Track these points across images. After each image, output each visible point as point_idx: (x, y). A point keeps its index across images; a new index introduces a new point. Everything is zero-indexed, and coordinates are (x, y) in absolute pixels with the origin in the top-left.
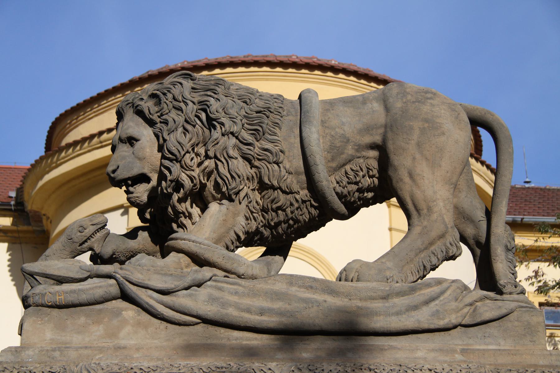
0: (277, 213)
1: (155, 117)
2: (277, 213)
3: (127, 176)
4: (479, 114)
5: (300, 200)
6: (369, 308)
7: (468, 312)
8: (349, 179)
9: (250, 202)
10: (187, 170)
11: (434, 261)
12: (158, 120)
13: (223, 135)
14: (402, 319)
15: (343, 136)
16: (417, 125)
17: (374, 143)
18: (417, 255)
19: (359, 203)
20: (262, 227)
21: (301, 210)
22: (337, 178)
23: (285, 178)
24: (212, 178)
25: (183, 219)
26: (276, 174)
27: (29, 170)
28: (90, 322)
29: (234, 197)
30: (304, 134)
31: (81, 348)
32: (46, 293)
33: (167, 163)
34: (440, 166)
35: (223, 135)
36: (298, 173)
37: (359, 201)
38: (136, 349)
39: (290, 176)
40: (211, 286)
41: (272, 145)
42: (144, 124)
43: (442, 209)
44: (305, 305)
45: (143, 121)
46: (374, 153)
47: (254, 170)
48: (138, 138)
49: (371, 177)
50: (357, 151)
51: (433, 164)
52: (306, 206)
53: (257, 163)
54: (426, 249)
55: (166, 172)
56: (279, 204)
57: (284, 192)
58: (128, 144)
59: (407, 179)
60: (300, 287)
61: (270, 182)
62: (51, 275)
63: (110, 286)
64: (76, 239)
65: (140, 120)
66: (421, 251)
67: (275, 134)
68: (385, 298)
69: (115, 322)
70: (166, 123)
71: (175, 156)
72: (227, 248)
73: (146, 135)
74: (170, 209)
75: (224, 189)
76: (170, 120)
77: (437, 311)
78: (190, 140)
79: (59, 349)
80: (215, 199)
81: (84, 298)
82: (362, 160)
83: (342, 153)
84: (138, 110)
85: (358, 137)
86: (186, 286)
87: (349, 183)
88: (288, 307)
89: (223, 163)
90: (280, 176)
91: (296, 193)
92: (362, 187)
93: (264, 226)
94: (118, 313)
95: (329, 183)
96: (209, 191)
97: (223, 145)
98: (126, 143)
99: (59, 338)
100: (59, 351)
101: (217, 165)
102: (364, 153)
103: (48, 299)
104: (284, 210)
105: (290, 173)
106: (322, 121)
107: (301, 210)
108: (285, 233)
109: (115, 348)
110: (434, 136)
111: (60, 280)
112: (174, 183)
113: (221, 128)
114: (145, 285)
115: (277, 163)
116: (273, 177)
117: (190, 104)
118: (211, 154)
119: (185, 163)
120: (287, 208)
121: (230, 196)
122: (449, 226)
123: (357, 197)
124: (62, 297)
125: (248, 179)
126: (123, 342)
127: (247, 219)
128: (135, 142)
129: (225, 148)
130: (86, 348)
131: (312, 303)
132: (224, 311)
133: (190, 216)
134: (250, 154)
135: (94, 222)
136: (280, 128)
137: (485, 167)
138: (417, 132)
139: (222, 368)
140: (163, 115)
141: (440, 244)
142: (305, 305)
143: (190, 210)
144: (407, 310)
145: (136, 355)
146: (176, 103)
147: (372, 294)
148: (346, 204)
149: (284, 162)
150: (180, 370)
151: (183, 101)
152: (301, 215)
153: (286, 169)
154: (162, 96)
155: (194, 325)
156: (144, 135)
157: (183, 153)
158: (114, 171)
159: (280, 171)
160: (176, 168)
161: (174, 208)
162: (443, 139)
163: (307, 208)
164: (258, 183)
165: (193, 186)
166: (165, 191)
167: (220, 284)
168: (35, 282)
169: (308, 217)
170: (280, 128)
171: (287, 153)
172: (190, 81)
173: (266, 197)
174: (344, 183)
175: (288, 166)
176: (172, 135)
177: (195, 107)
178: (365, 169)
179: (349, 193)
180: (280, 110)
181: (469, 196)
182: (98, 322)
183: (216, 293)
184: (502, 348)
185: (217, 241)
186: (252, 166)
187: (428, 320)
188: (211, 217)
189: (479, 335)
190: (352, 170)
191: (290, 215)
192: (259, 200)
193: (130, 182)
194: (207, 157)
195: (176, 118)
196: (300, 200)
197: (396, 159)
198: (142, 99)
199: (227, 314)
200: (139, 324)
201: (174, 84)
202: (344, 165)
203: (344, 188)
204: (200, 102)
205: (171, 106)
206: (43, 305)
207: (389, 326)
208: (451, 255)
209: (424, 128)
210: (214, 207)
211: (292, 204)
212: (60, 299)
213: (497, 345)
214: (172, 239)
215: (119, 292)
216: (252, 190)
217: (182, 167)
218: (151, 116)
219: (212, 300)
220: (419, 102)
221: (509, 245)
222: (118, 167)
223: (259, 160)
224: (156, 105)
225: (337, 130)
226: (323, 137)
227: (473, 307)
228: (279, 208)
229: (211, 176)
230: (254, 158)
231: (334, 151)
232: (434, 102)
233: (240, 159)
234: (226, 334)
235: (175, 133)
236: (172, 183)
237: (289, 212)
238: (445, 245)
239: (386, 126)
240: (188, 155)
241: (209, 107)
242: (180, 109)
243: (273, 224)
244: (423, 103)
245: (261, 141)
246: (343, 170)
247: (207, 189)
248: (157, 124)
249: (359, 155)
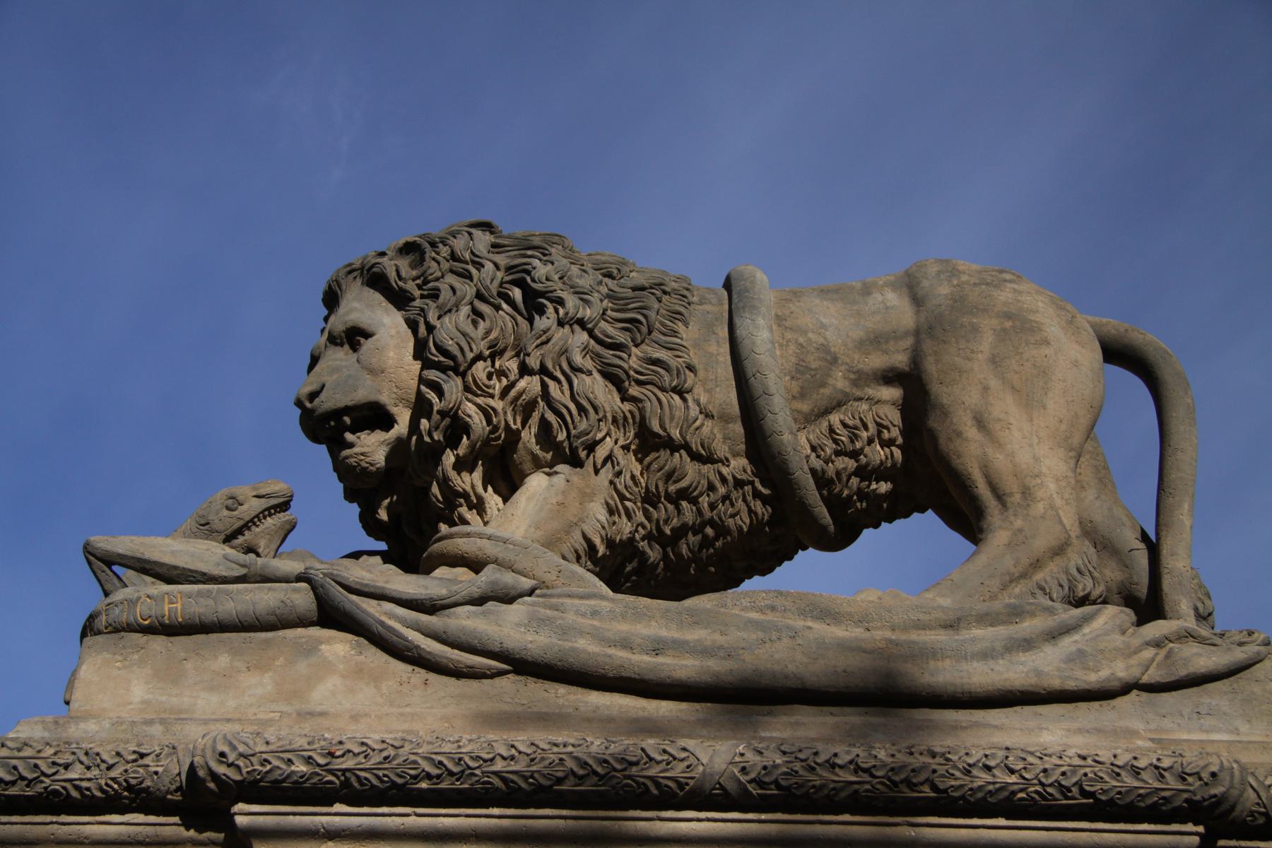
0: (678, 507)
1: (411, 286)
2: (678, 507)
3: (341, 404)
4: (1113, 331)
5: (730, 478)
6: (914, 643)
7: (1153, 660)
8: (837, 444)
9: (619, 474)
10: (477, 396)
12: (417, 293)
13: (561, 324)
14: (997, 668)
15: (824, 348)
16: (988, 325)
17: (892, 369)
18: (1004, 587)
19: (858, 504)
20: (643, 539)
21: (732, 505)
22: (811, 437)
23: (698, 423)
24: (536, 416)
25: (463, 510)
26: (679, 413)
28: (240, 665)
29: (583, 454)
30: (740, 332)
31: (216, 720)
32: (139, 598)
33: (433, 375)
34: (1044, 407)
35: (561, 324)
36: (725, 418)
37: (860, 500)
38: (351, 717)
39: (709, 423)
41: (669, 353)
42: (385, 303)
43: (1055, 496)
44: (761, 635)
45: (382, 298)
46: (892, 393)
47: (627, 407)
48: (370, 329)
49: (887, 444)
50: (855, 383)
51: (1030, 402)
52: (744, 495)
53: (634, 391)
54: (1024, 575)
55: (432, 396)
56: (683, 484)
57: (695, 457)
58: (347, 347)
59: (972, 432)
61: (665, 430)
62: (155, 563)
64: (217, 525)
65: (378, 297)
66: (1014, 580)
67: (675, 333)
68: (952, 625)
69: (302, 667)
71: (453, 358)
74: (435, 489)
75: (562, 436)
78: (488, 332)
79: (163, 721)
80: (538, 465)
82: (865, 406)
83: (823, 384)
84: (375, 273)
85: (856, 356)
86: (476, 595)
87: (838, 453)
88: (720, 639)
89: (559, 382)
90: (686, 419)
91: (721, 461)
92: (867, 464)
93: (648, 537)
96: (526, 448)
97: (561, 343)
98: (342, 345)
99: (164, 699)
100: (160, 723)
101: (544, 386)
102: (870, 392)
104: (694, 501)
105: (709, 416)
106: (777, 316)
107: (732, 505)
108: (695, 559)
109: (299, 714)
110: (1027, 344)
112: (447, 421)
113: (557, 311)
114: (378, 591)
115: (681, 392)
116: (672, 419)
118: (533, 362)
119: (474, 380)
120: (701, 494)
121: (574, 451)
122: (1073, 535)
123: (855, 487)
124: (179, 606)
125: (615, 421)
127: (611, 511)
128: (362, 340)
129: (564, 351)
130: (228, 720)
131: (779, 630)
132: (568, 645)
134: (620, 367)
135: (263, 491)
136: (686, 324)
139: (565, 746)
140: (429, 282)
141: (1055, 570)
142: (761, 635)
143: (480, 490)
147: (921, 616)
148: (833, 502)
149: (695, 391)
150: (459, 747)
151: (474, 263)
152: (733, 516)
153: (699, 405)
154: (428, 248)
155: (492, 676)
156: (384, 325)
157: (470, 356)
159: (687, 408)
160: (453, 386)
161: (445, 483)
163: (745, 500)
164: (636, 436)
165: (491, 432)
166: (427, 439)
167: (553, 600)
168: (116, 581)
169: (748, 521)
170: (686, 324)
171: (701, 374)
173: (655, 466)
174: (828, 451)
175: (703, 400)
176: (446, 319)
177: (500, 275)
178: (872, 428)
179: (838, 473)
180: (686, 293)
181: (1103, 497)
182: (262, 668)
184: (1245, 739)
185: (550, 543)
187: (1059, 669)
188: (529, 499)
189: (1186, 712)
190: (845, 425)
191: (708, 514)
192: (637, 473)
193: (347, 420)
194: (524, 370)
196: (730, 478)
197: (942, 392)
199: (573, 649)
200: (358, 672)
202: (827, 411)
203: (826, 462)
204: (509, 269)
207: (965, 681)
208: (1081, 594)
209: (1004, 330)
210: (536, 483)
211: (711, 487)
213: (1232, 732)
215: (314, 606)
216: (623, 447)
217: (467, 389)
218: (400, 283)
219: (538, 622)
220: (987, 284)
221: (1200, 605)
222: (323, 386)
223: (640, 383)
224: (413, 266)
225: (810, 335)
226: (781, 345)
227: (1163, 652)
228: (684, 494)
229: (530, 416)
230: (628, 376)
231: (807, 377)
233: (596, 375)
234: (572, 697)
235: (453, 316)
236: (443, 419)
237: (706, 505)
238: (1067, 572)
239: (917, 333)
240: (480, 364)
241: (529, 273)
243: (668, 532)
244: (997, 287)
245: (644, 347)
247: (520, 445)
248: (414, 299)
249: (858, 393)
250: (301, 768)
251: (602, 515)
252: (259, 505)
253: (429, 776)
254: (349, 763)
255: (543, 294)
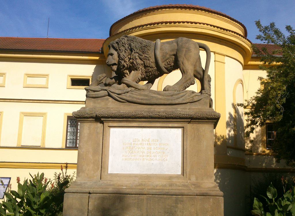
11: (188, 85)
12: (118, 49)
13: (134, 53)
16: (184, 49)
27: (105, 41)
29: (137, 69)
35: (134, 53)
40: (130, 93)
46: (174, 57)
50: (170, 56)
51: (188, 60)
56: (149, 71)
57: (151, 68)
60: (151, 93)
63: (105, 93)
66: (184, 83)
67: (148, 52)
70: (120, 50)
71: (122, 59)
72: (137, 83)
73: (115, 53)
76: (121, 49)
77: (184, 99)
81: (99, 96)
82: (171, 59)
83: (166, 57)
87: (168, 65)
94: (108, 99)
95: (162, 65)
102: (172, 57)
103: (91, 96)
105: (152, 63)
111: (94, 91)
117: (126, 44)
118: (132, 58)
126: (109, 107)
132: (133, 99)
133: (127, 74)
137: (246, 40)
138: (184, 52)
144: (177, 99)
145: (112, 110)
146: (123, 44)
158: (108, 63)
162: (191, 53)
167: (132, 92)
172: (127, 38)
178: (172, 61)
180: (150, 46)
183: (131, 95)
185: (133, 81)
186: (142, 61)
195: (122, 49)
198: (114, 43)
201: (122, 39)
205: (121, 45)
206: (91, 97)
209: (186, 50)
210: (133, 72)
211: (153, 71)
212: (94, 96)
214: (123, 80)
220: (186, 43)
228: (150, 72)
231: (164, 56)
232: (190, 43)
242: (124, 46)
246: (166, 61)
249: (170, 57)
250: (107, 115)
251: (140, 75)
252: (103, 77)
253: (118, 116)
254: (111, 115)
255: (133, 49)
